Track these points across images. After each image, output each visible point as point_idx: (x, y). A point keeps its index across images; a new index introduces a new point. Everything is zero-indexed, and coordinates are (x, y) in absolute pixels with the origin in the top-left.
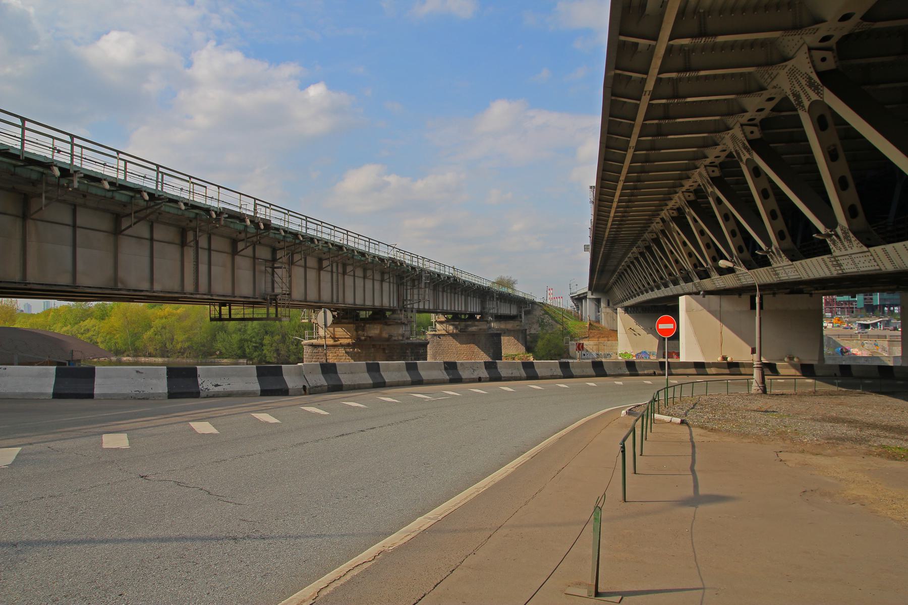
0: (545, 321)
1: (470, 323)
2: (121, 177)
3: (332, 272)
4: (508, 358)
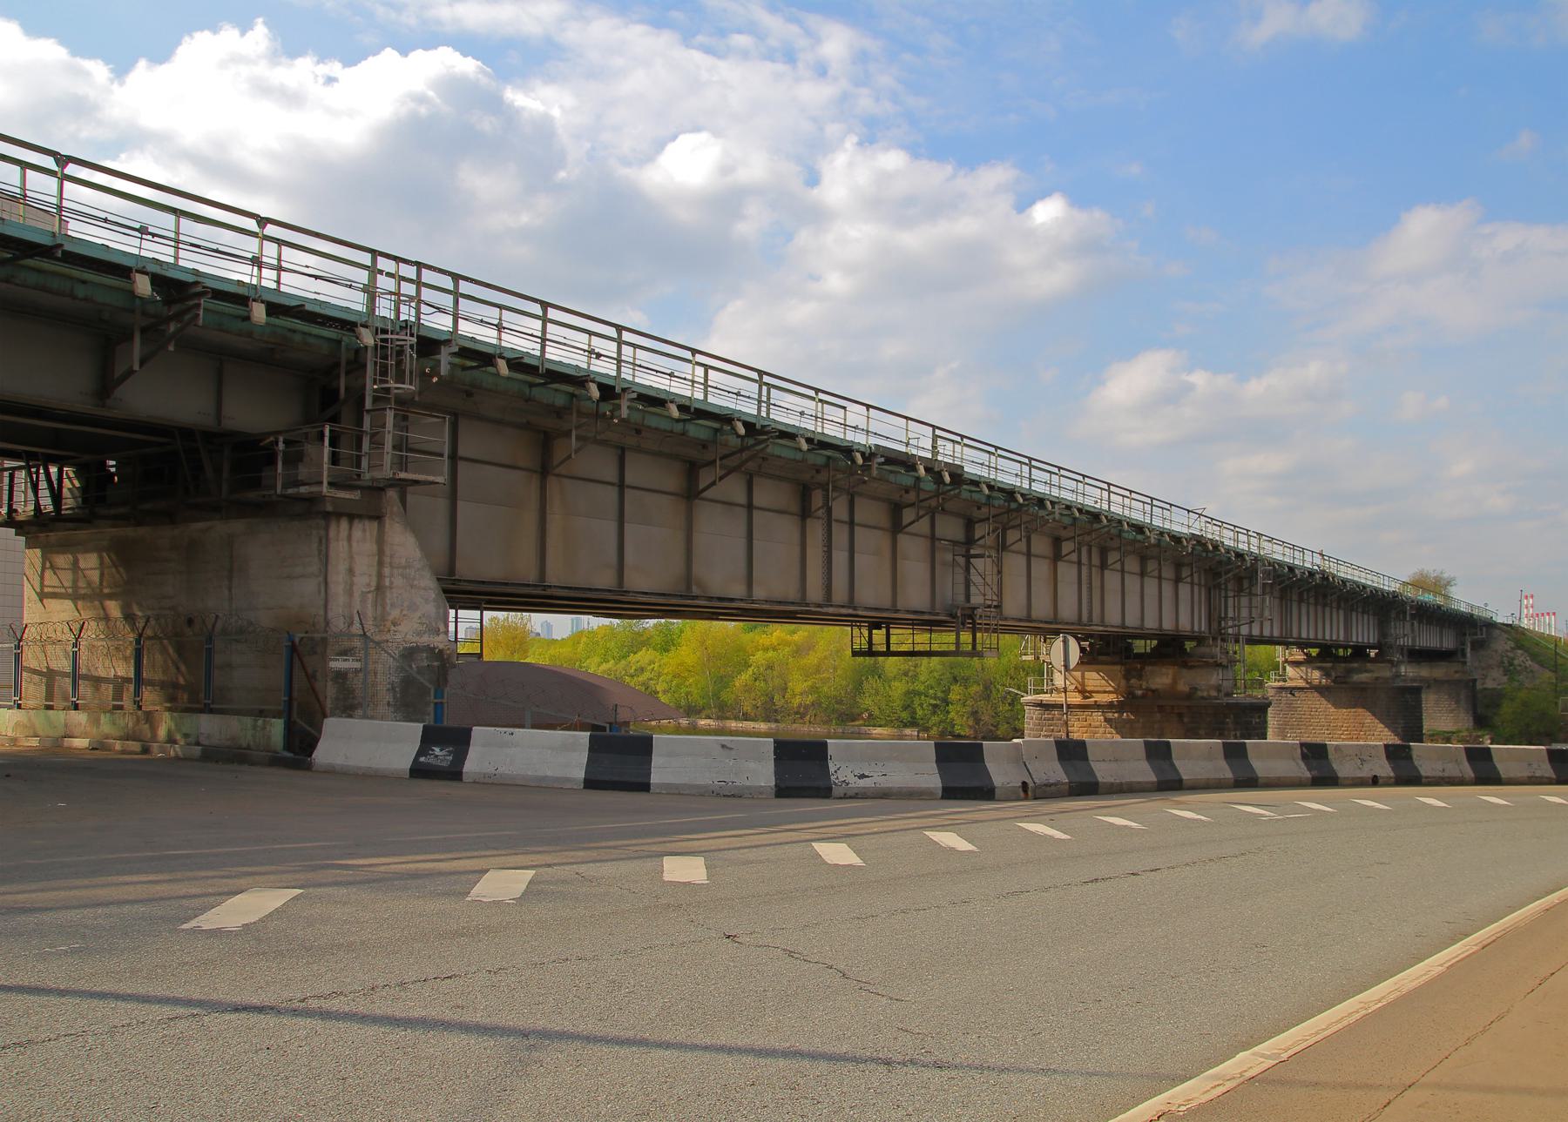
3: (1079, 563)
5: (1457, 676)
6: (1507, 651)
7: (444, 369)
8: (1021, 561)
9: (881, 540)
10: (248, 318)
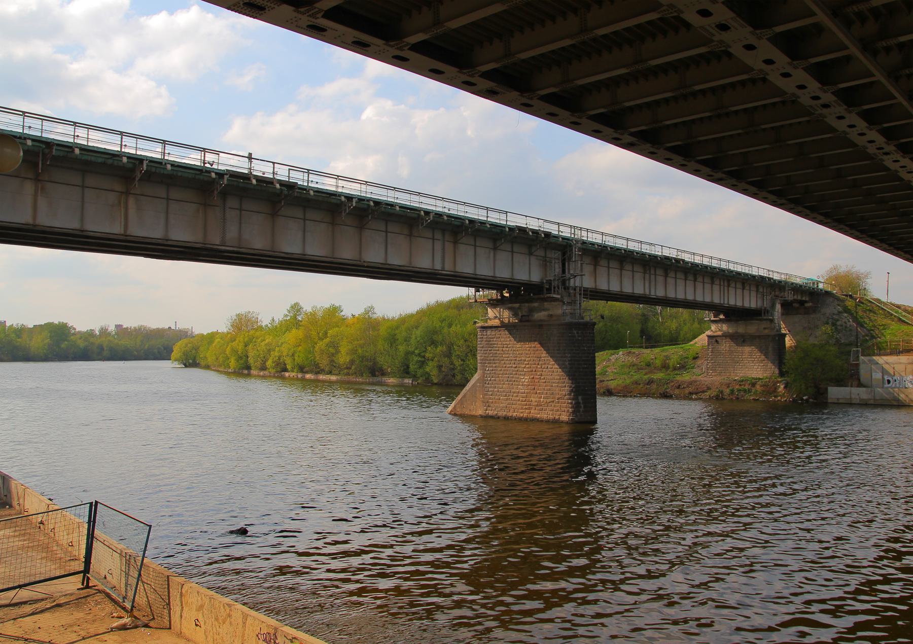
0: (838, 323)
1: (536, 305)
2: (306, 184)
3: (720, 285)
4: (744, 383)
5: (766, 331)
6: (834, 314)
7: (226, 182)
8: (748, 292)
9: (741, 291)
10: (122, 161)
